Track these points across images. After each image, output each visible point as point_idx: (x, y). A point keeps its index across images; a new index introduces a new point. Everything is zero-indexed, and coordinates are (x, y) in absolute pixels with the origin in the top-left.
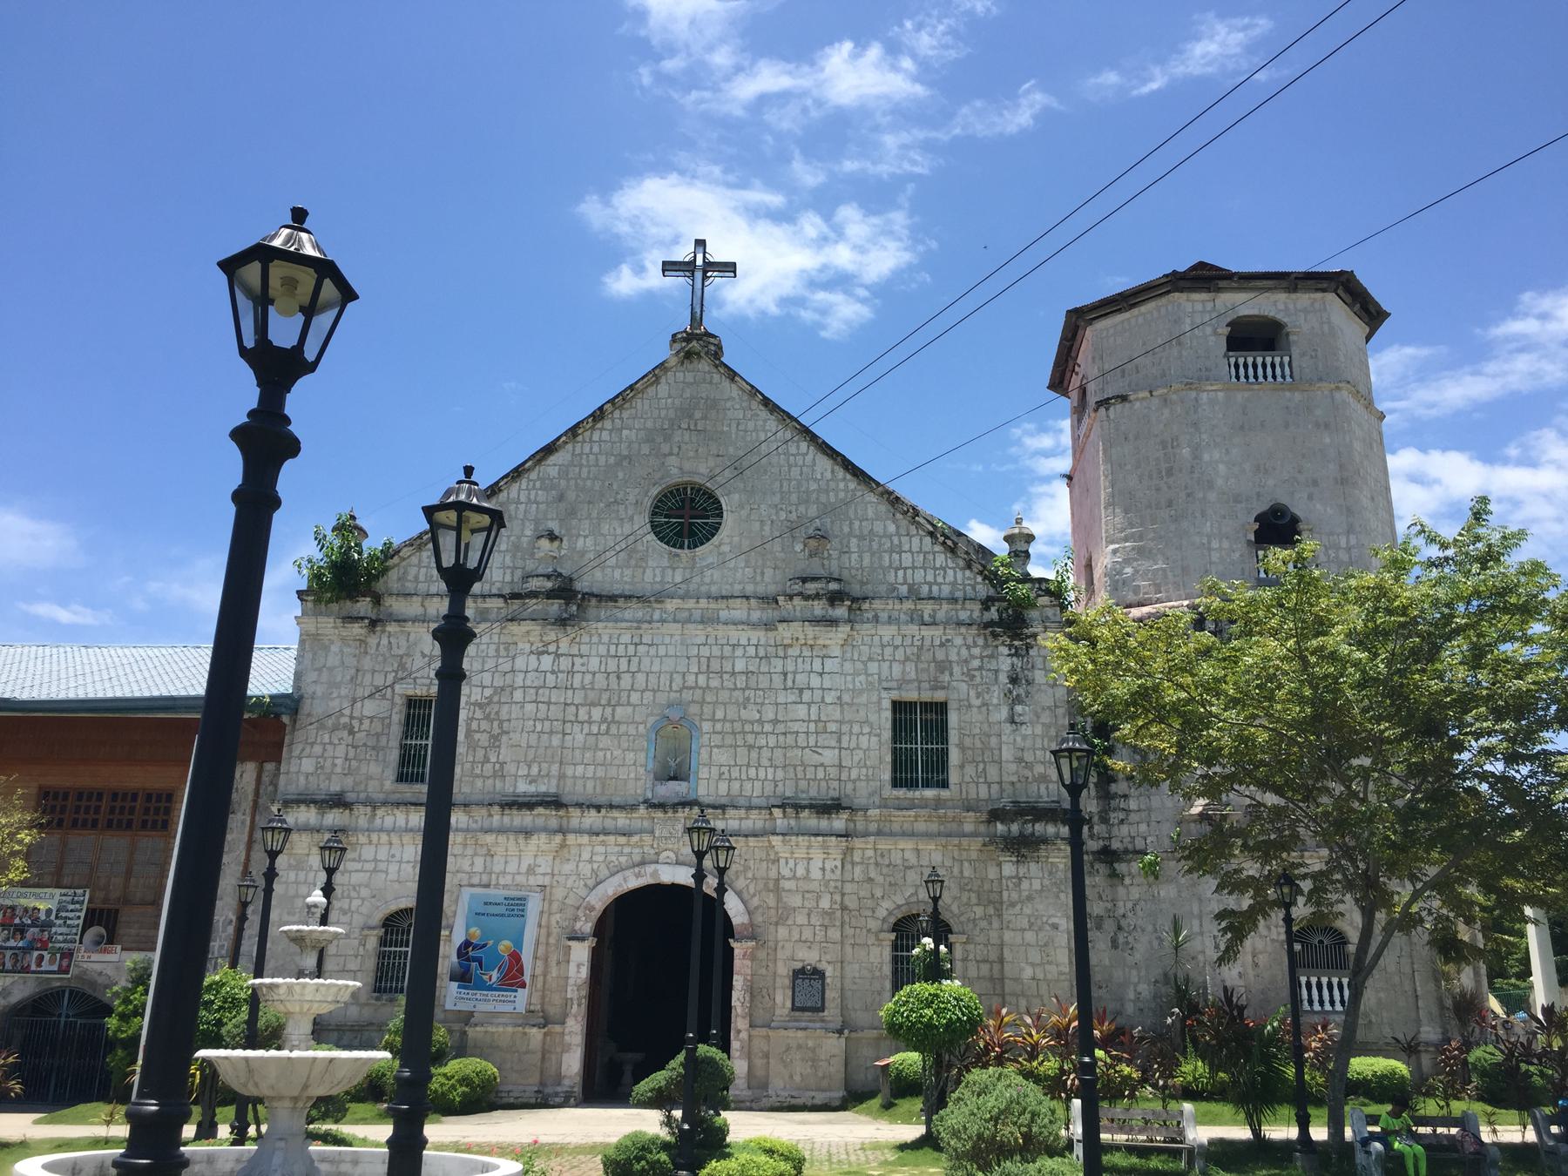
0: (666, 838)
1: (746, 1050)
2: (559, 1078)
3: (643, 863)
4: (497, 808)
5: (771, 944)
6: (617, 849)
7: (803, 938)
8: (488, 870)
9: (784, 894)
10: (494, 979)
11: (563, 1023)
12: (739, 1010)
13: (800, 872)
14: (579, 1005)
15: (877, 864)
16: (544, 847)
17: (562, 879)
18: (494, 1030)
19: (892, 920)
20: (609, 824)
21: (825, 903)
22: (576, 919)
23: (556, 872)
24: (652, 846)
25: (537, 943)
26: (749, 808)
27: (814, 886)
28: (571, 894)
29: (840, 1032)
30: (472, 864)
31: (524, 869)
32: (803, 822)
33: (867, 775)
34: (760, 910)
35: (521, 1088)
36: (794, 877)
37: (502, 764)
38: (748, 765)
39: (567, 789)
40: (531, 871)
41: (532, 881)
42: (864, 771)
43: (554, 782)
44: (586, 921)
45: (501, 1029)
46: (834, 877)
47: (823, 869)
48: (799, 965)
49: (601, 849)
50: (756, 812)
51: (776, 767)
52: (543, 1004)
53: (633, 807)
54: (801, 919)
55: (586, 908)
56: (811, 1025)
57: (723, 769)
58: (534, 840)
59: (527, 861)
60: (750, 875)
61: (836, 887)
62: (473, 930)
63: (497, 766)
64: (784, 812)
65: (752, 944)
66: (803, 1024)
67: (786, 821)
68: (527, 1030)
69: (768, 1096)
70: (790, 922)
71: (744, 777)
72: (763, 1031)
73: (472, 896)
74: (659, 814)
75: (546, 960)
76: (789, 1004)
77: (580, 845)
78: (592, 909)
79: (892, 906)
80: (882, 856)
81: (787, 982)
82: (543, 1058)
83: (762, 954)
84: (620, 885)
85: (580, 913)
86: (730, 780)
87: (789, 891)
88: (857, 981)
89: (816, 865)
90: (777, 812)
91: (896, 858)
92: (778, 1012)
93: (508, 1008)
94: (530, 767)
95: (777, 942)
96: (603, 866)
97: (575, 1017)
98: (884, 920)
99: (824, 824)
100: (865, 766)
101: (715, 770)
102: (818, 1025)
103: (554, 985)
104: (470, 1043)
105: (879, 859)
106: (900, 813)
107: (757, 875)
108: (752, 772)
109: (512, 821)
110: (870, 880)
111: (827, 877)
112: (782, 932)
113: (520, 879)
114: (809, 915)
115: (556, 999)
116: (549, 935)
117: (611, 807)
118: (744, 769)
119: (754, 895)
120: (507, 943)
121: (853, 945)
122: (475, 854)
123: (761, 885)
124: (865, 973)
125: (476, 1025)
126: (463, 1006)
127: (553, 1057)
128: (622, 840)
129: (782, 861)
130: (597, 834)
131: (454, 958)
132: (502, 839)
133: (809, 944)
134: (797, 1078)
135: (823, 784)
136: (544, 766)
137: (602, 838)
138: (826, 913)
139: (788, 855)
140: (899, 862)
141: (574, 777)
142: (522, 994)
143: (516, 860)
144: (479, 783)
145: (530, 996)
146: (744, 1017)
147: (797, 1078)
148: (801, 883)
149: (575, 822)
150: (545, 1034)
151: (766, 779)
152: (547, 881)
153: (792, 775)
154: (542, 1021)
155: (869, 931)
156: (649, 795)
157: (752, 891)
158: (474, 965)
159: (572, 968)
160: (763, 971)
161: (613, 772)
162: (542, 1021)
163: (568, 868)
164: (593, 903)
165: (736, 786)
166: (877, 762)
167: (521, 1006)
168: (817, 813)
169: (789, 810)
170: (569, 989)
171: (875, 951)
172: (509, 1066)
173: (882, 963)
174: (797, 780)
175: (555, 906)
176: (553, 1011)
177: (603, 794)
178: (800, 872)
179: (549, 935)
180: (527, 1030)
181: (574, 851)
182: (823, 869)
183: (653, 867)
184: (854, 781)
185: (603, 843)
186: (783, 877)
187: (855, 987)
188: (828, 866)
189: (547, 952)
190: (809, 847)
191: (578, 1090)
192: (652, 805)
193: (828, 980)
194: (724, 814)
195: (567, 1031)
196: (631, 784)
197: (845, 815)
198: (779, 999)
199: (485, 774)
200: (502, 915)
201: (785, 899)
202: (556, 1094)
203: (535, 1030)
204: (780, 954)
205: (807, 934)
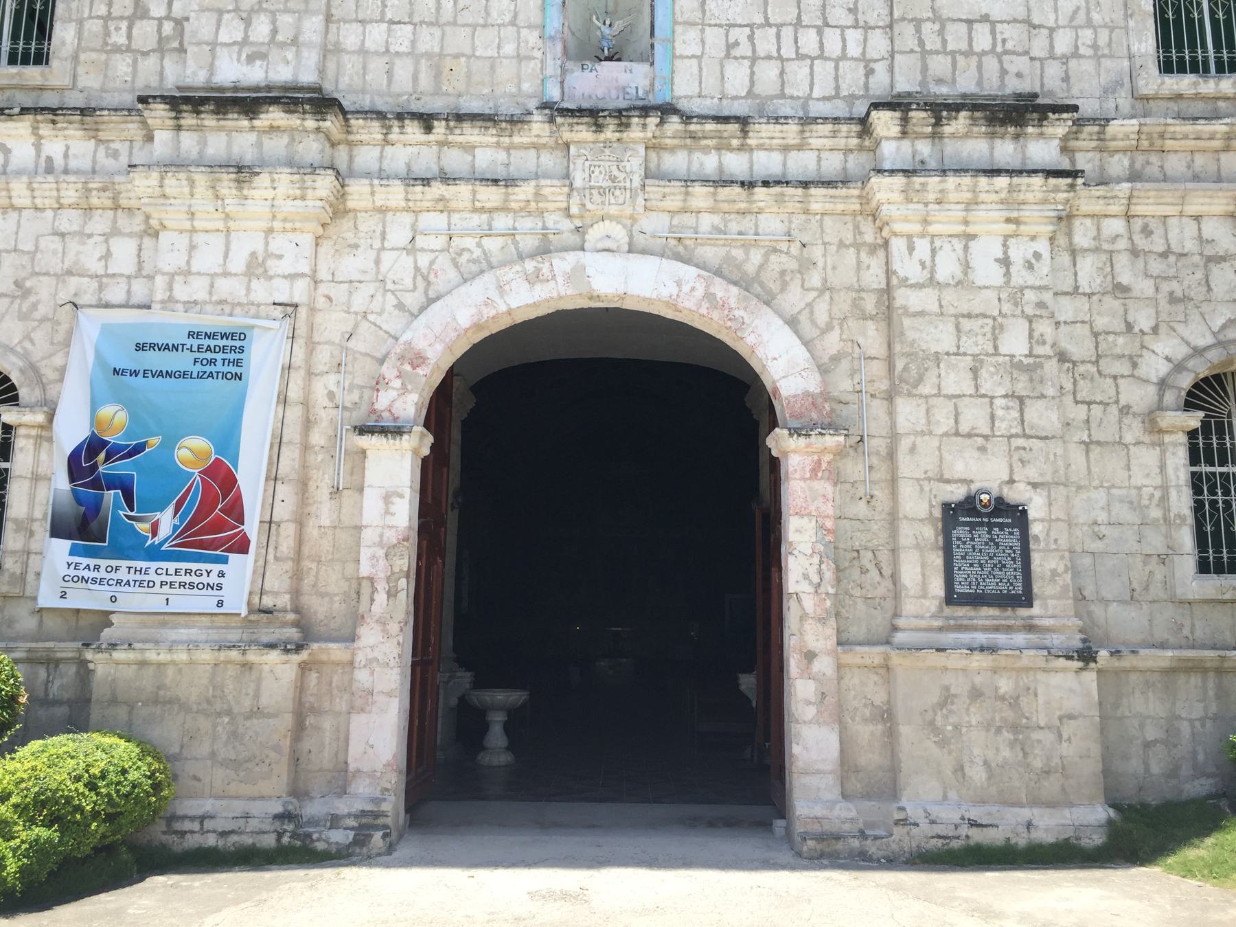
0: (602, 192)
1: (830, 700)
2: (341, 777)
3: (544, 250)
4: (159, 111)
5: (878, 444)
6: (477, 220)
7: (964, 428)
8: (148, 269)
9: (907, 322)
10: (165, 530)
11: (352, 638)
12: (809, 603)
13: (947, 268)
14: (392, 594)
15: (1135, 252)
16: (288, 207)
17: (339, 292)
18: (164, 657)
19: (1186, 382)
20: (455, 160)
21: (1015, 343)
22: (378, 383)
23: (323, 274)
24: (567, 212)
25: (278, 443)
26: (807, 121)
27: (986, 302)
28: (364, 325)
29: (1086, 655)
30: (107, 256)
31: (238, 263)
32: (950, 147)
33: (1095, 47)
34: (845, 365)
35: (239, 807)
36: (932, 282)
37: (180, 23)
38: (798, 24)
39: (344, 81)
40: (256, 268)
41: (261, 292)
42: (1087, 35)
43: (311, 58)
44: (404, 390)
45: (182, 656)
46: (1031, 280)
47: (1005, 262)
48: (957, 493)
49: (436, 221)
50: (827, 128)
51: (867, 28)
52: (296, 593)
53: (517, 121)
54: (955, 380)
55: (402, 358)
56: (1001, 638)
57: (735, 34)
58: (261, 186)
59: (245, 245)
60: (815, 280)
61: (1041, 305)
62: (107, 411)
63: (168, 27)
64: (905, 120)
65: (832, 441)
66: (981, 638)
67: (906, 145)
68: (252, 657)
69: (903, 822)
70: (926, 389)
71: (788, 51)
72: (874, 655)
73: (107, 331)
74: (582, 133)
75: (303, 485)
76: (937, 587)
77: (383, 211)
78: (418, 360)
79: (1181, 352)
80: (1147, 232)
81: (930, 533)
82: (299, 728)
83: (854, 469)
84: (488, 302)
85: (388, 370)
86: (754, 59)
87: (922, 314)
88: (1103, 530)
89: (986, 252)
90: (885, 122)
91: (1183, 236)
92: (910, 606)
93: (203, 602)
94: (248, 22)
95: (894, 437)
96: (443, 261)
97: (382, 622)
98: (1163, 384)
99: (1005, 150)
100: (1089, 24)
101: (715, 38)
102: (1020, 638)
103: (326, 545)
104: (99, 690)
105: (1141, 242)
106: (1188, 128)
107: (835, 281)
108: (809, 41)
109: (203, 143)
110: (1121, 290)
111: (1017, 280)
112: (908, 413)
113: (226, 288)
114: (975, 371)
115: (333, 580)
116: (308, 424)
117: (460, 118)
118: (787, 33)
119: (829, 328)
120: (198, 443)
121: (1087, 445)
122: (115, 232)
123: (844, 302)
124: (1124, 513)
125: (113, 646)
126: (80, 599)
127: (327, 724)
128: (490, 196)
129: (898, 245)
130: (426, 182)
131: (62, 482)
132: (175, 184)
133: (983, 441)
134: (977, 774)
135: (991, 64)
136: (286, 20)
137: (437, 189)
138: (1019, 366)
139: (916, 228)
140: (1190, 246)
141: (363, 52)
142: (239, 568)
143: (218, 241)
144: (122, 66)
145: (262, 572)
146: (822, 621)
147: (977, 774)
148: (949, 296)
149: (367, 157)
150: (304, 667)
151: (844, 56)
152: (299, 292)
153: (912, 43)
154: (293, 633)
155: (1125, 410)
156: (554, 93)
157: (822, 317)
158: (110, 495)
159: (371, 504)
160: (861, 509)
161: (458, 40)
162: (293, 633)
163: (354, 265)
164: (421, 344)
165: (768, 74)
166: (1118, 16)
167: (236, 598)
168: (991, 121)
169: (916, 115)
170: (365, 554)
171: (1147, 458)
172: (205, 749)
173: (1165, 488)
174: (925, 53)
175: (323, 357)
176: (319, 608)
177: (437, 92)
178: (947, 268)
179: (308, 424)
180: (252, 657)
181: (368, 224)
182: (1005, 262)
183: (572, 257)
184: (1065, 59)
185: (443, 207)
186: (904, 282)
187: (1097, 546)
188: (1018, 252)
189: (304, 466)
190: (972, 204)
191: (393, 806)
192: (554, 111)
193: (1036, 529)
194: (745, 133)
195: (360, 657)
196: (506, 70)
197: (1059, 128)
198: (910, 574)
199: (137, 44)
200: (184, 375)
201: (911, 335)
202: (335, 821)
203: (274, 656)
204: (907, 467)
205: (975, 416)
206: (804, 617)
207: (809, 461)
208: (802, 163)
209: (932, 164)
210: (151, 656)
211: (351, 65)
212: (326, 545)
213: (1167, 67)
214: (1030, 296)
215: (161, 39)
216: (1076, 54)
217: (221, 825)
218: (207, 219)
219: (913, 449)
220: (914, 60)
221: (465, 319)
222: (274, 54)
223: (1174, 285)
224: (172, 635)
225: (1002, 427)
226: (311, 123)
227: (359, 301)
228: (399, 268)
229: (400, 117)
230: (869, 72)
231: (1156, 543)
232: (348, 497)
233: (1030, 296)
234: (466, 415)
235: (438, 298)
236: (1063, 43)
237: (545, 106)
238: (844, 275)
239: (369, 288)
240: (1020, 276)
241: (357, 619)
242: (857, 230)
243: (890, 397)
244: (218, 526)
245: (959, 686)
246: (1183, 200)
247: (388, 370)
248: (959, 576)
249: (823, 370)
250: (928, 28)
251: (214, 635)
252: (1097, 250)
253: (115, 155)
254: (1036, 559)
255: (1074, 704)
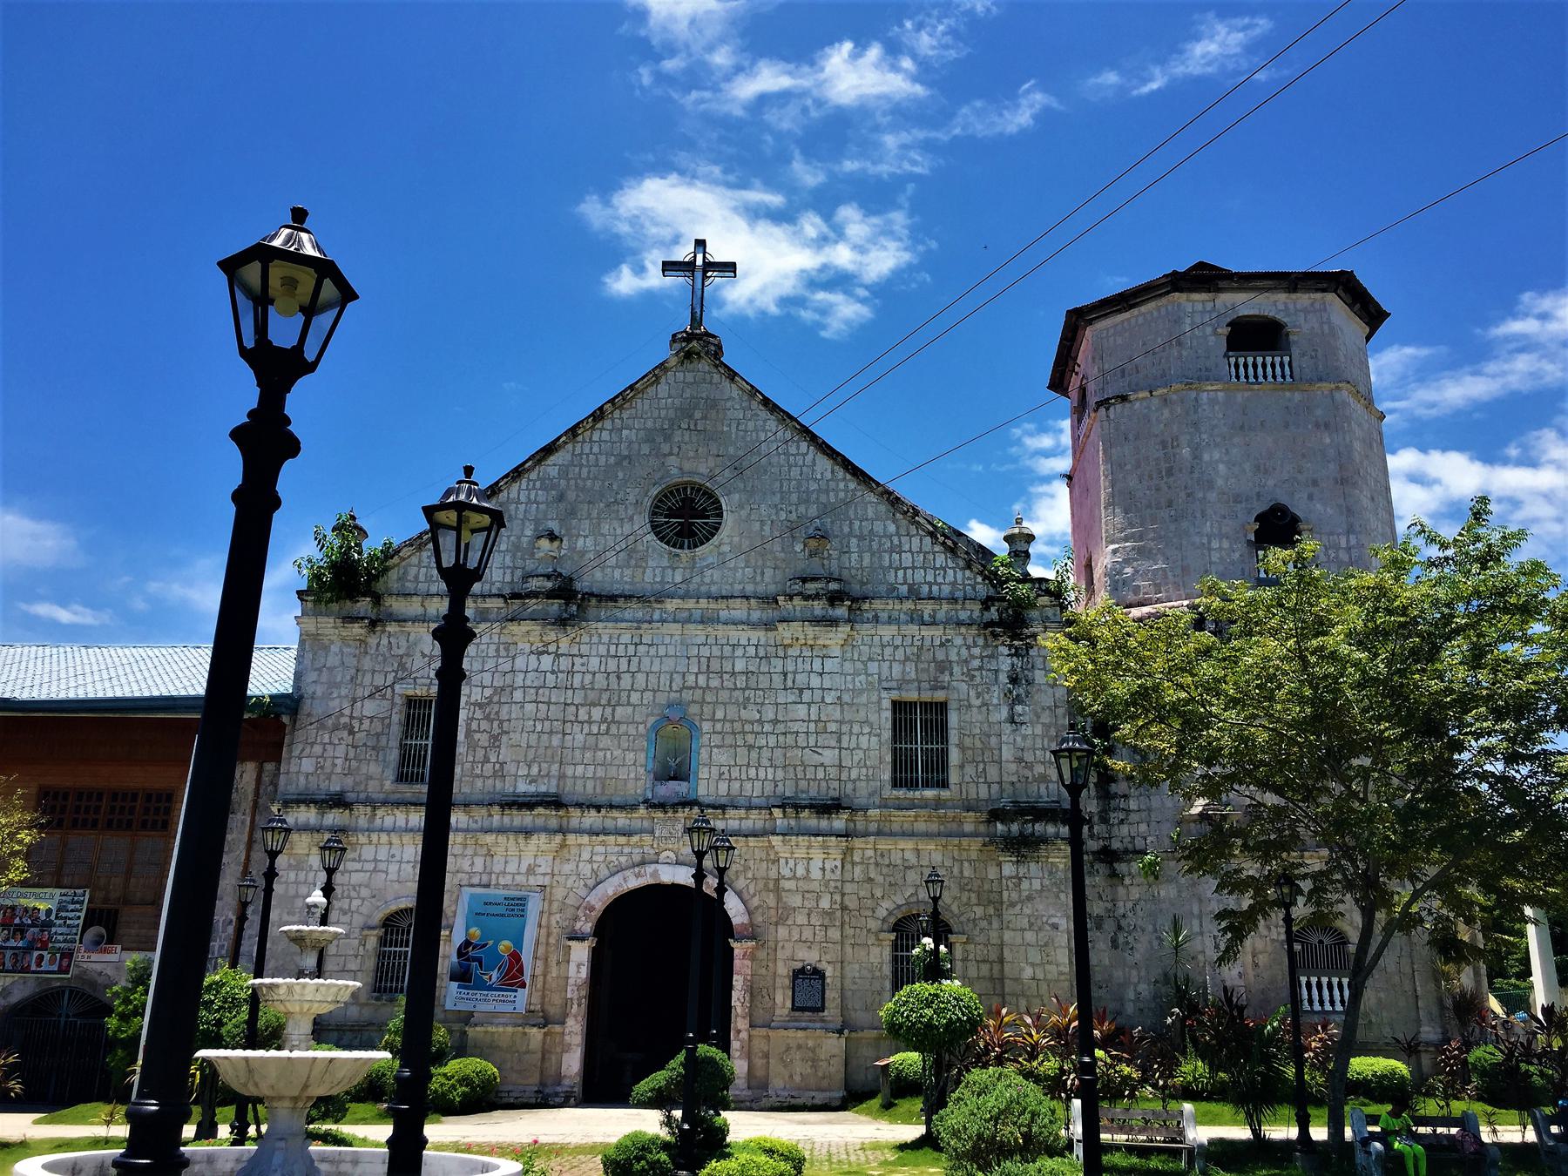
1: (746, 1049)
2: (559, 1079)
3: (643, 863)
5: (771, 944)
6: (617, 849)
7: (803, 939)
8: (488, 870)
11: (563, 1023)
12: (739, 1010)
13: (800, 871)
14: (579, 1005)
15: (877, 864)
16: (544, 847)
17: (562, 879)
18: (494, 1030)
19: (892, 920)
20: (609, 824)
21: (825, 903)
22: (576, 919)
23: (556, 872)
25: (537, 943)
27: (815, 886)
29: (840, 1032)
31: (524, 869)
36: (794, 877)
40: (531, 871)
41: (532, 881)
42: (864, 771)
43: (554, 782)
47: (823, 869)
48: (799, 965)
49: (601, 849)
50: (757, 812)
51: (776, 767)
52: (542, 1004)
54: (801, 919)
56: (811, 1025)
58: (534, 839)
60: (750, 875)
61: (836, 887)
62: (472, 930)
63: (497, 766)
64: (784, 812)
70: (790, 922)
71: (744, 777)
72: (763, 1031)
76: (789, 1004)
77: (580, 845)
78: (592, 909)
80: (882, 856)
81: (787, 982)
83: (762, 954)
84: (620, 885)
86: (730, 780)
89: (816, 865)
91: (896, 858)
92: (778, 1012)
93: (508, 1008)
97: (575, 1016)
98: (884, 920)
99: (824, 824)
101: (715, 770)
103: (554, 985)
104: (470, 1043)
108: (752, 772)
110: (871, 880)
111: (827, 877)
112: (782, 932)
113: (520, 879)
114: (809, 915)
115: (556, 999)
116: (549, 935)
118: (744, 768)
119: (755, 895)
122: (476, 854)
123: (761, 885)
124: (865, 973)
128: (622, 840)
129: (782, 861)
130: (597, 835)
132: (502, 839)
133: (809, 944)
135: (824, 784)
136: (545, 766)
137: (602, 838)
138: (827, 913)
141: (574, 777)
142: (522, 994)
144: (479, 783)
147: (797, 1078)
148: (801, 883)
151: (766, 779)
154: (542, 1020)
155: (869, 931)
156: (649, 795)
157: (752, 891)
159: (572, 967)
160: (763, 971)
161: (613, 772)
162: (542, 1020)
164: (593, 903)
169: (788, 810)
170: (569, 989)
171: (875, 951)
175: (555, 906)
178: (800, 871)
181: (574, 851)
182: (823, 869)
184: (854, 781)
185: (603, 843)
186: (783, 877)
187: (854, 987)
189: (547, 952)
192: (651, 805)
193: (828, 980)
195: (567, 1030)
196: (631, 785)
198: (779, 998)
199: (485, 774)
203: (535, 1030)
204: (780, 954)
205: (808, 934)
206: (737, 1016)
207: (742, 952)
208: (748, 825)
209: (796, 829)
210: (490, 1029)
211: (569, 782)
212: (554, 985)
213: (896, 783)
214: (832, 883)
215: (495, 772)
216: (859, 779)
217: (515, 1095)
218: (513, 850)
219: (783, 947)
220: (793, 782)
221: (610, 892)
222: (540, 780)
223: (891, 879)
224: (497, 1021)
225: (818, 938)
226: (554, 813)
227: (570, 883)
228: (586, 869)
229: (588, 807)
230: (776, 786)
231: (877, 986)
232: (563, 966)
233: (832, 883)
234: (465, 665)
235: (601, 882)
236: (854, 775)
237: (646, 801)
238: (761, 873)
239: (574, 878)
240: (828, 875)
241: (565, 1015)
242: (768, 854)
243: (777, 924)
244: (515, 977)
245: (793, 1044)
246: (896, 844)
247: (580, 914)
248: (797, 999)
249: (750, 913)
250: (799, 768)
251: (513, 1021)
252: (862, 863)
253: (476, 822)
254: (827, 992)
255: (835, 1051)
